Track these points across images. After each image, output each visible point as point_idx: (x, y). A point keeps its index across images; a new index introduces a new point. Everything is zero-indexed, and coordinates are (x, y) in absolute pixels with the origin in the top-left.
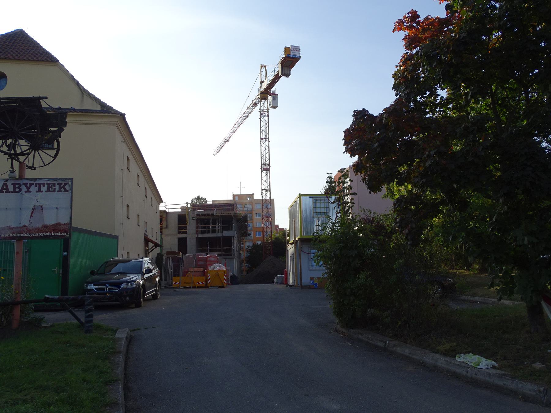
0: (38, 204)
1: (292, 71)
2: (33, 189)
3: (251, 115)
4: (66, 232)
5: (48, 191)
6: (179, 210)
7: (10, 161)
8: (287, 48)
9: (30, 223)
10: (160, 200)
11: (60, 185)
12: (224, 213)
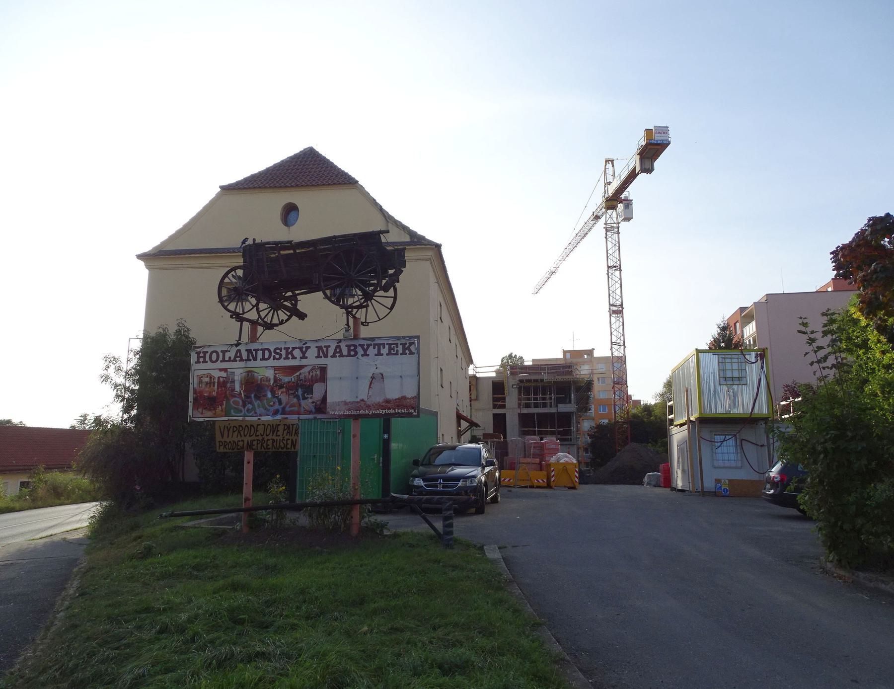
0: (378, 371)
1: (657, 164)
2: (372, 351)
3: (589, 234)
4: (413, 408)
5: (389, 354)
6: (494, 375)
7: (345, 315)
8: (648, 132)
9: (369, 397)
10: (470, 361)
11: (404, 345)
12: (559, 378)
